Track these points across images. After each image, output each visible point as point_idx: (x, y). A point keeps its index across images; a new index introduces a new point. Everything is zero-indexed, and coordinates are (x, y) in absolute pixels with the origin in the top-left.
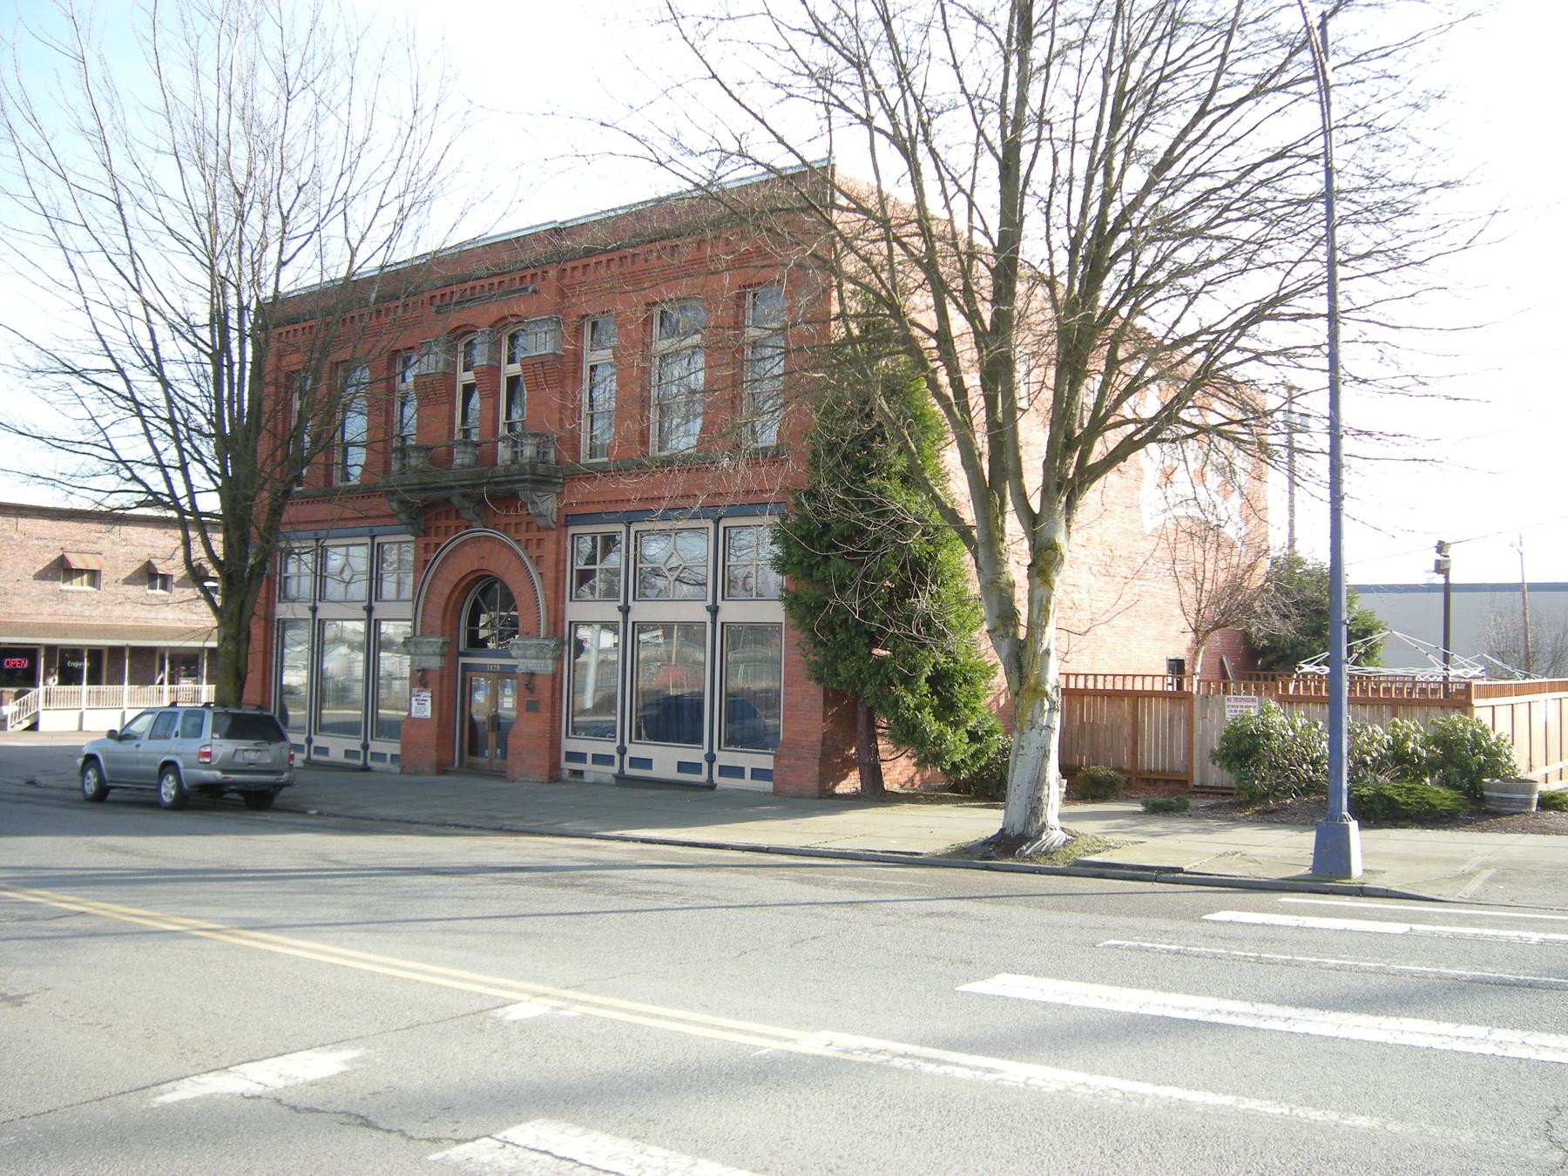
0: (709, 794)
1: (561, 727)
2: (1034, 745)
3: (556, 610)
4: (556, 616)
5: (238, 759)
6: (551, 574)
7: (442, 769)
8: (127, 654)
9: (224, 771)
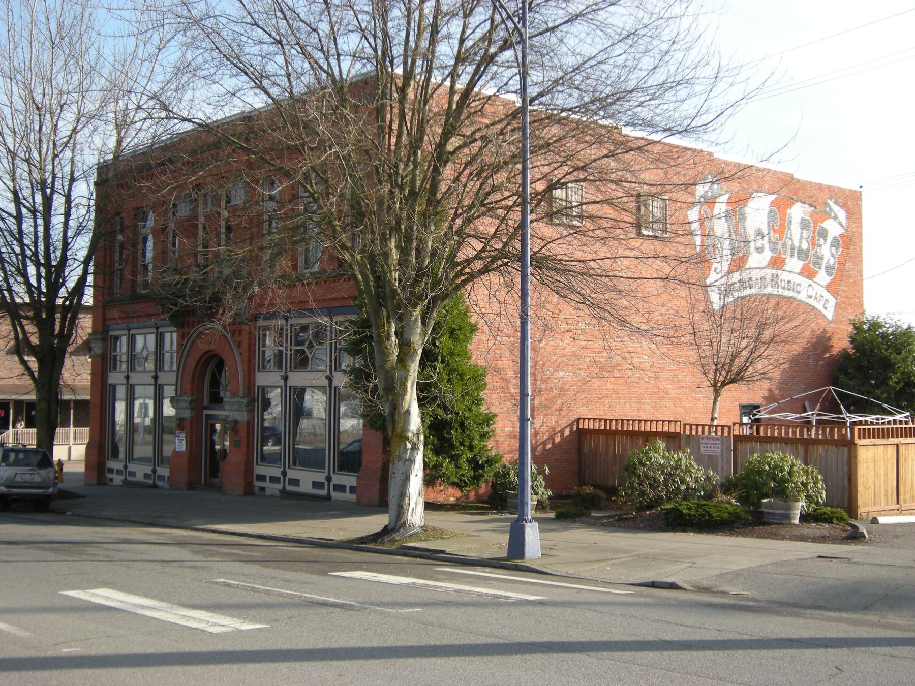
0: (328, 503)
1: (253, 458)
2: (401, 472)
3: (249, 378)
4: (249, 382)
5: (18, 479)
6: (246, 354)
7: (192, 486)
8: (72, 406)
9: (7, 487)
